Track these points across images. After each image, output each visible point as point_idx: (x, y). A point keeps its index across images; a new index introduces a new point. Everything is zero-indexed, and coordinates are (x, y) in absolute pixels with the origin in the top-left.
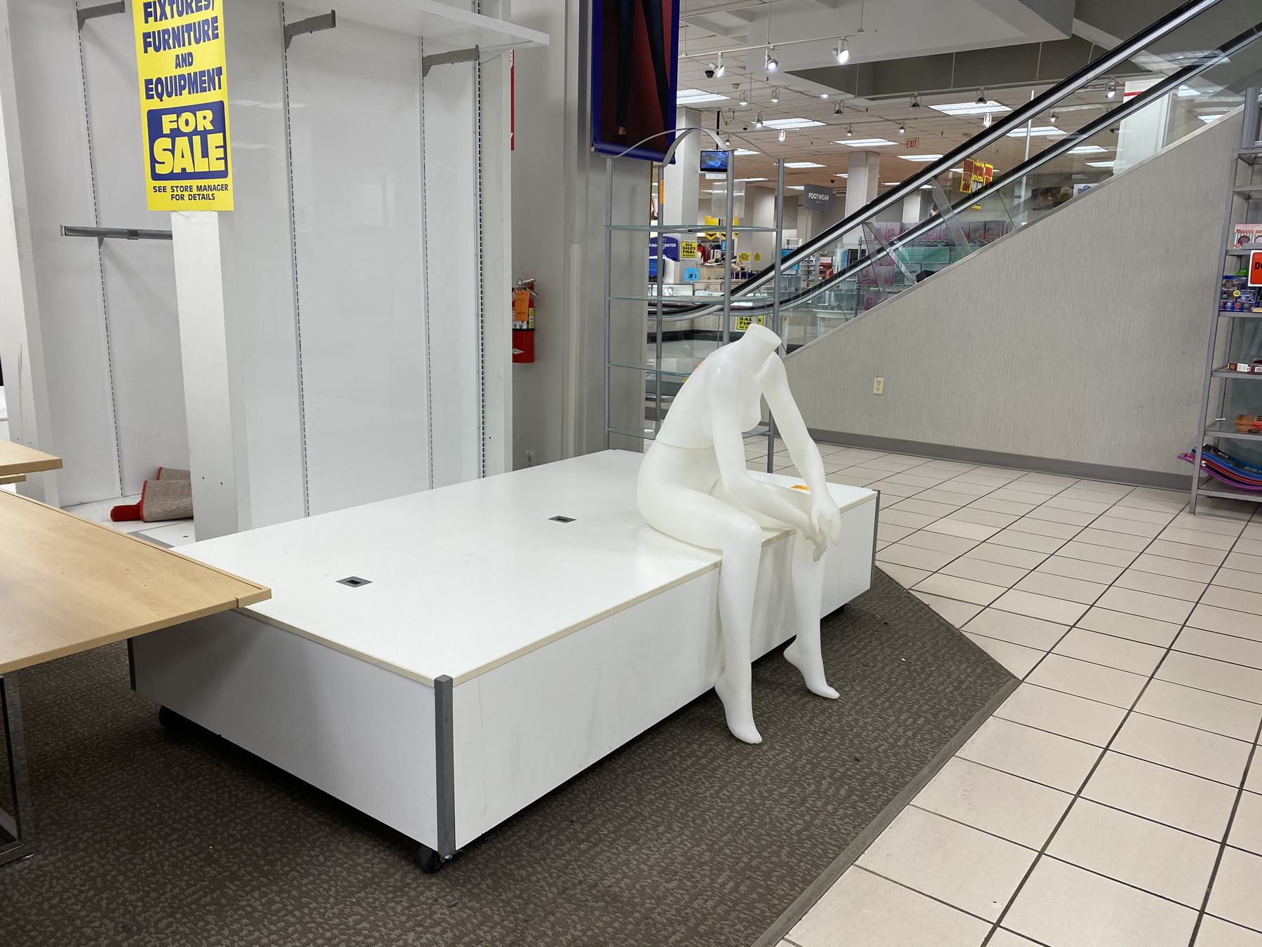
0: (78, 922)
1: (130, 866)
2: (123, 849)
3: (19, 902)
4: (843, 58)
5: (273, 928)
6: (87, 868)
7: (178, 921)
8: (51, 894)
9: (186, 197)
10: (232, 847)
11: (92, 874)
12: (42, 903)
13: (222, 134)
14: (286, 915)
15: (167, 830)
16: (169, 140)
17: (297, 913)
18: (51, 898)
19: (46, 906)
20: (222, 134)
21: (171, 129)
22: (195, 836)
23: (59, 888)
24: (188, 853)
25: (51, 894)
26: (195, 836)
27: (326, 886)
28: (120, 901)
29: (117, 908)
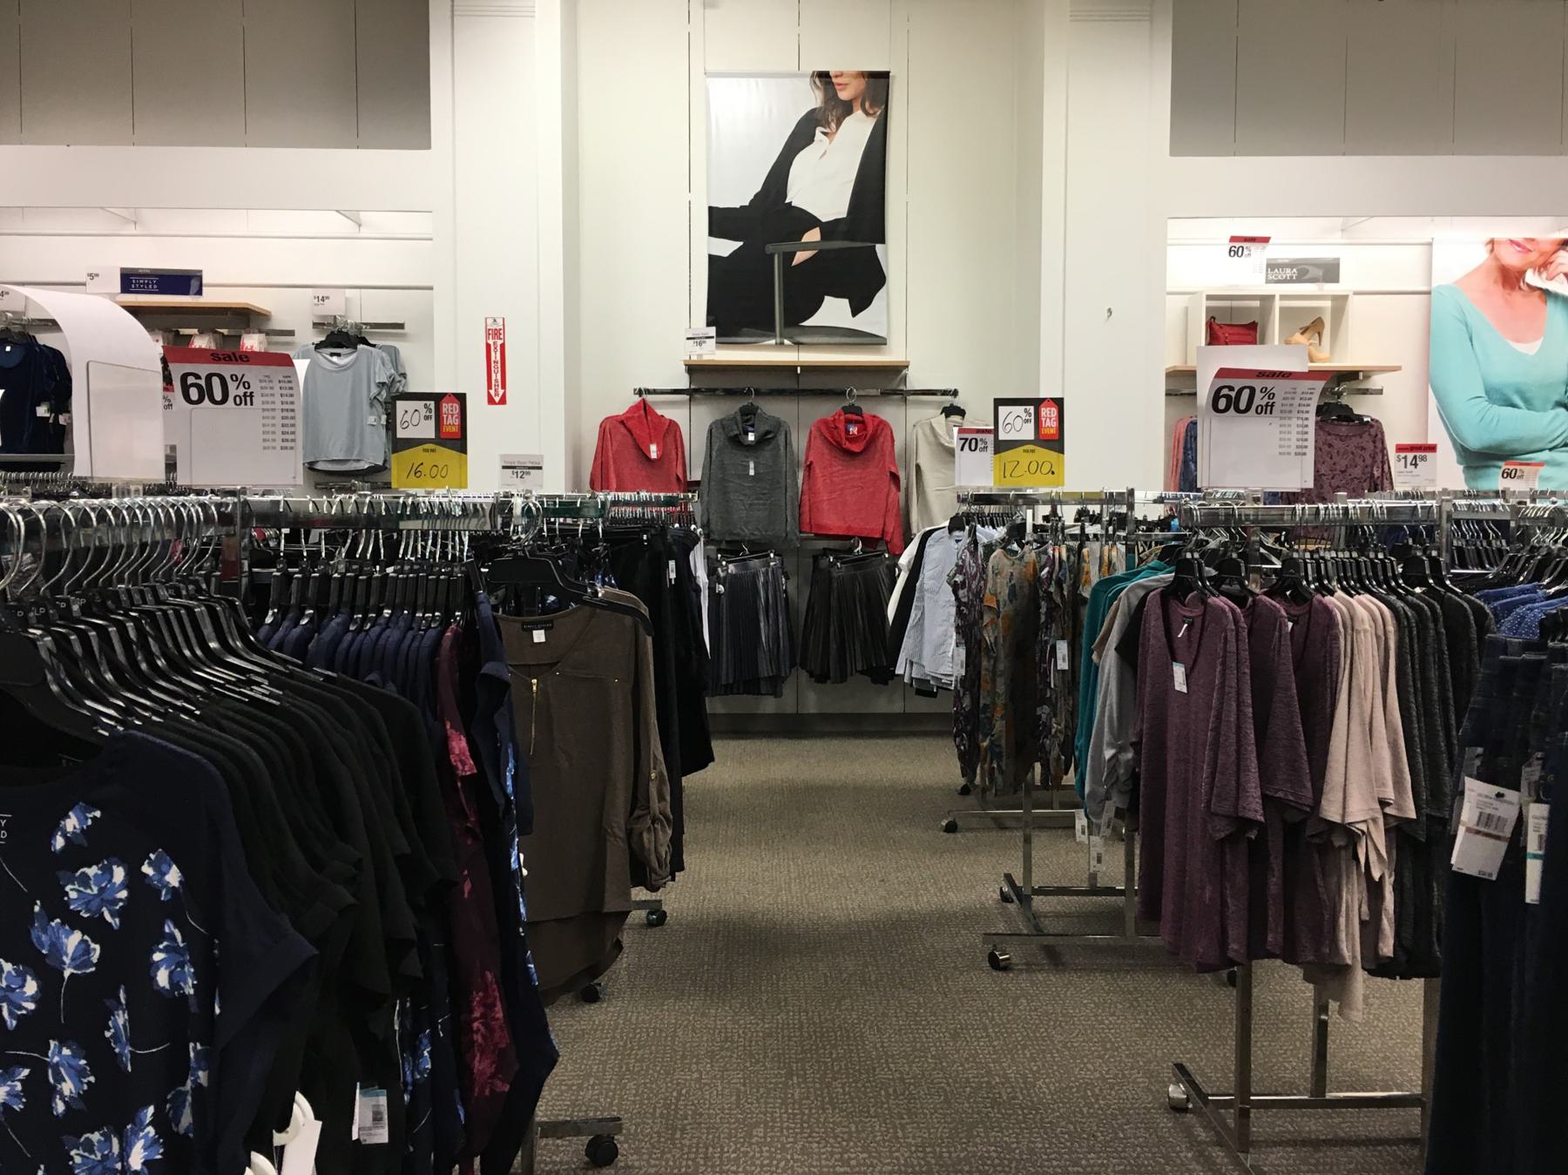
22: (1189, 1044)
26: (1189, 1044)
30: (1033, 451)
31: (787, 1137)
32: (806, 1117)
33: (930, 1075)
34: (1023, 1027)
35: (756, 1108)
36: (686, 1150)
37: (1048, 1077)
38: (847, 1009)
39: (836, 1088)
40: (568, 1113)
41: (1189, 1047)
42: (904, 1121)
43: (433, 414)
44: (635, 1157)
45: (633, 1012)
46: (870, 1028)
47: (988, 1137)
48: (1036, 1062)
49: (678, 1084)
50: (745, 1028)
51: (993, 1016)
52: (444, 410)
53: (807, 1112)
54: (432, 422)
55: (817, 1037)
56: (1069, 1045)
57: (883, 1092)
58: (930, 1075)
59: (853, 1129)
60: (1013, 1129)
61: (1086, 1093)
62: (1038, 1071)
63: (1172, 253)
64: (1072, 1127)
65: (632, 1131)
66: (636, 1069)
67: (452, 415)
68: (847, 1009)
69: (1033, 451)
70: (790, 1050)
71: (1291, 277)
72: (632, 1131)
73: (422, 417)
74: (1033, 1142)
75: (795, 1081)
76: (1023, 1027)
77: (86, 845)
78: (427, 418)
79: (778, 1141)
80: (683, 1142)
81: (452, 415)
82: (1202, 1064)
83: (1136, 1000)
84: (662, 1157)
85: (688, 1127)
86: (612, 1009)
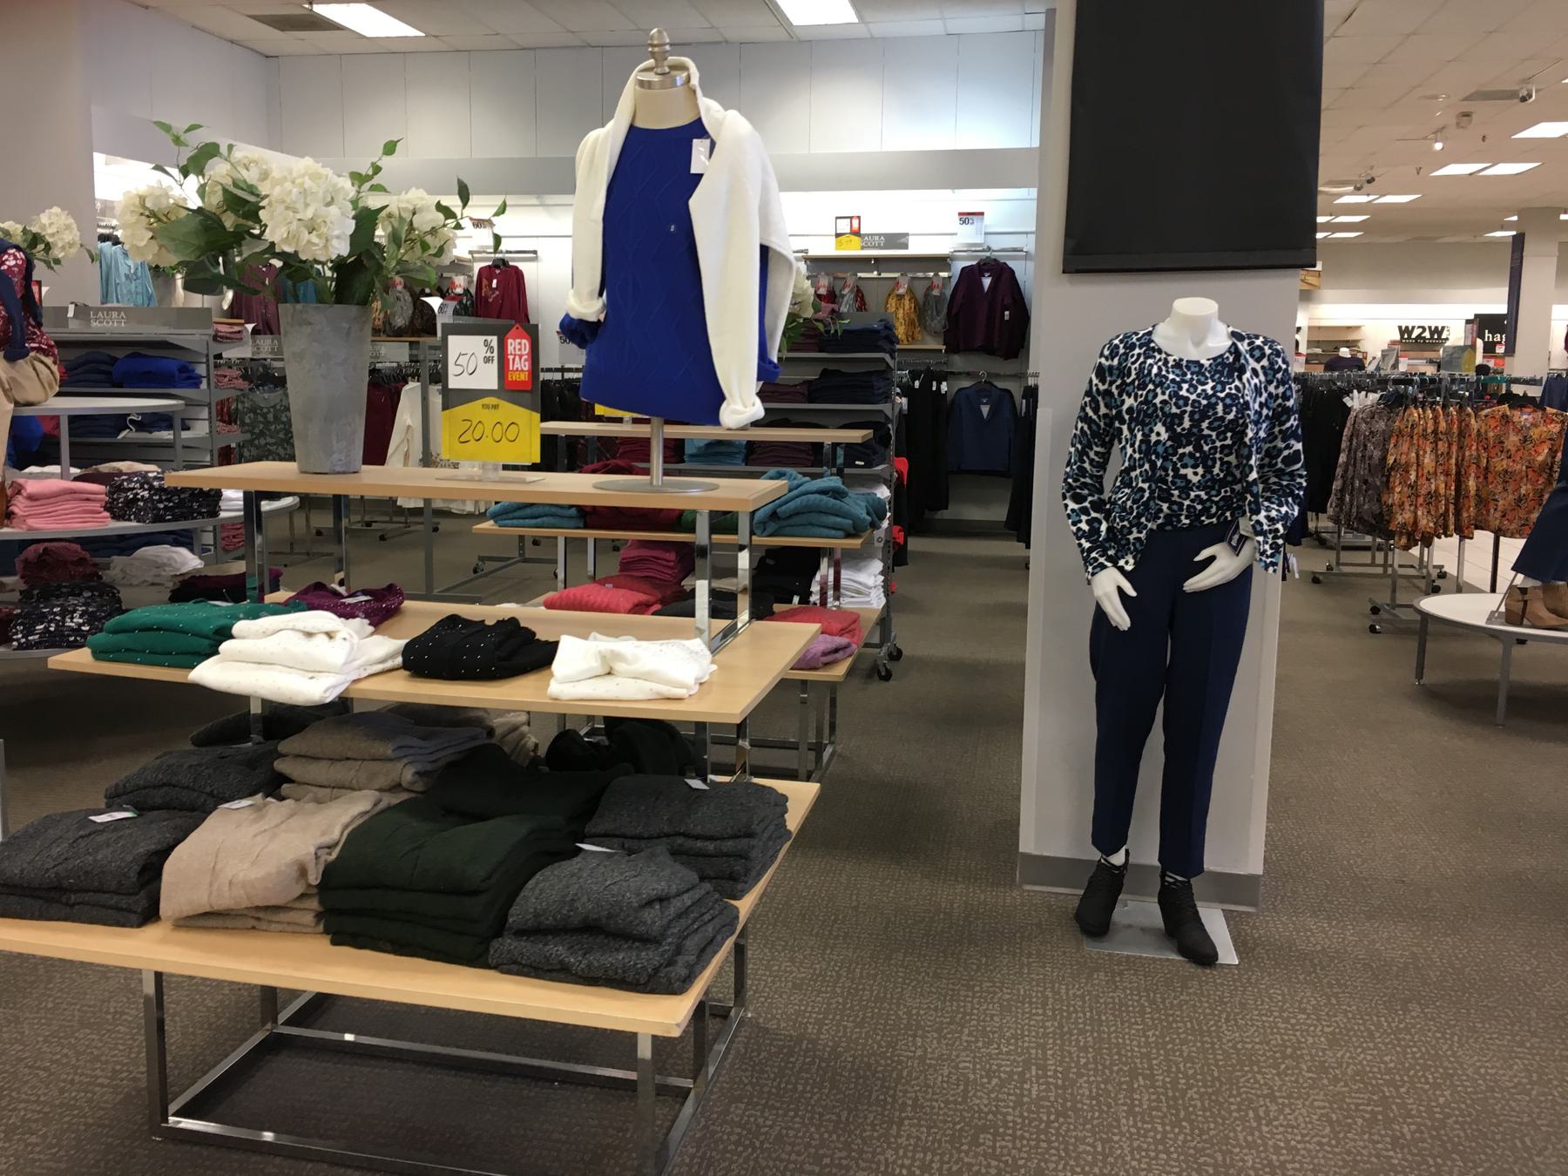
0: (1256, 1069)
1: (1320, 1054)
2: (1322, 1039)
3: (1223, 1032)
4: (566, 461)
5: (1139, 1124)
6: (1286, 1038)
7: (1332, 1108)
8: (1248, 1040)
9: (703, 525)
10: (1419, 1085)
11: (1288, 1044)
12: (1480, 1067)
13: (538, 460)
14: (1428, 1156)
15: (1371, 1045)
16: (1382, 562)
17: (1168, 1128)
18: (1247, 1043)
19: (1483, 1071)
20: (538, 460)
21: (1512, 569)
22: (1391, 1061)
23: (1498, 1065)
24: (1376, 1070)
25: (1248, 1040)
26: (1391, 1061)
27: (1483, 1157)
28: (1296, 1071)
29: (1292, 1075)
30: (495, 407)
31: (1020, 1151)
32: (1043, 1125)
33: (957, 1056)
34: (1188, 1016)
35: (986, 1106)
36: (901, 1152)
37: (1205, 1086)
38: (1195, 993)
39: (1081, 1087)
40: (775, 1084)
41: (1392, 1065)
42: (1282, 1158)
43: (495, 354)
44: (844, 1154)
45: (857, 964)
46: (1227, 1020)
47: (994, 1148)
48: (1194, 1063)
49: (900, 1062)
50: (980, 997)
51: (1380, 1021)
52: (510, 349)
53: (1045, 1118)
54: (494, 367)
55: (1062, 1017)
56: (1483, 1071)
57: (1251, 1114)
58: (957, 1056)
59: (1099, 1149)
60: (1147, 1150)
61: (1247, 1115)
62: (1194, 1076)
63: (200, 296)
64: (1220, 1158)
65: (843, 1119)
66: (854, 1036)
67: (521, 356)
68: (1195, 993)
69: (495, 407)
70: (1131, 1041)
71: (879, 244)
72: (843, 1119)
73: (481, 361)
74: (1046, 1161)
75: (1034, 1073)
76: (1188, 1016)
77: (607, 743)
78: (487, 360)
79: (1009, 1155)
80: (899, 1141)
81: (521, 356)
82: (1403, 1090)
83: (1336, 995)
84: (874, 1157)
85: (906, 1122)
86: (835, 957)
